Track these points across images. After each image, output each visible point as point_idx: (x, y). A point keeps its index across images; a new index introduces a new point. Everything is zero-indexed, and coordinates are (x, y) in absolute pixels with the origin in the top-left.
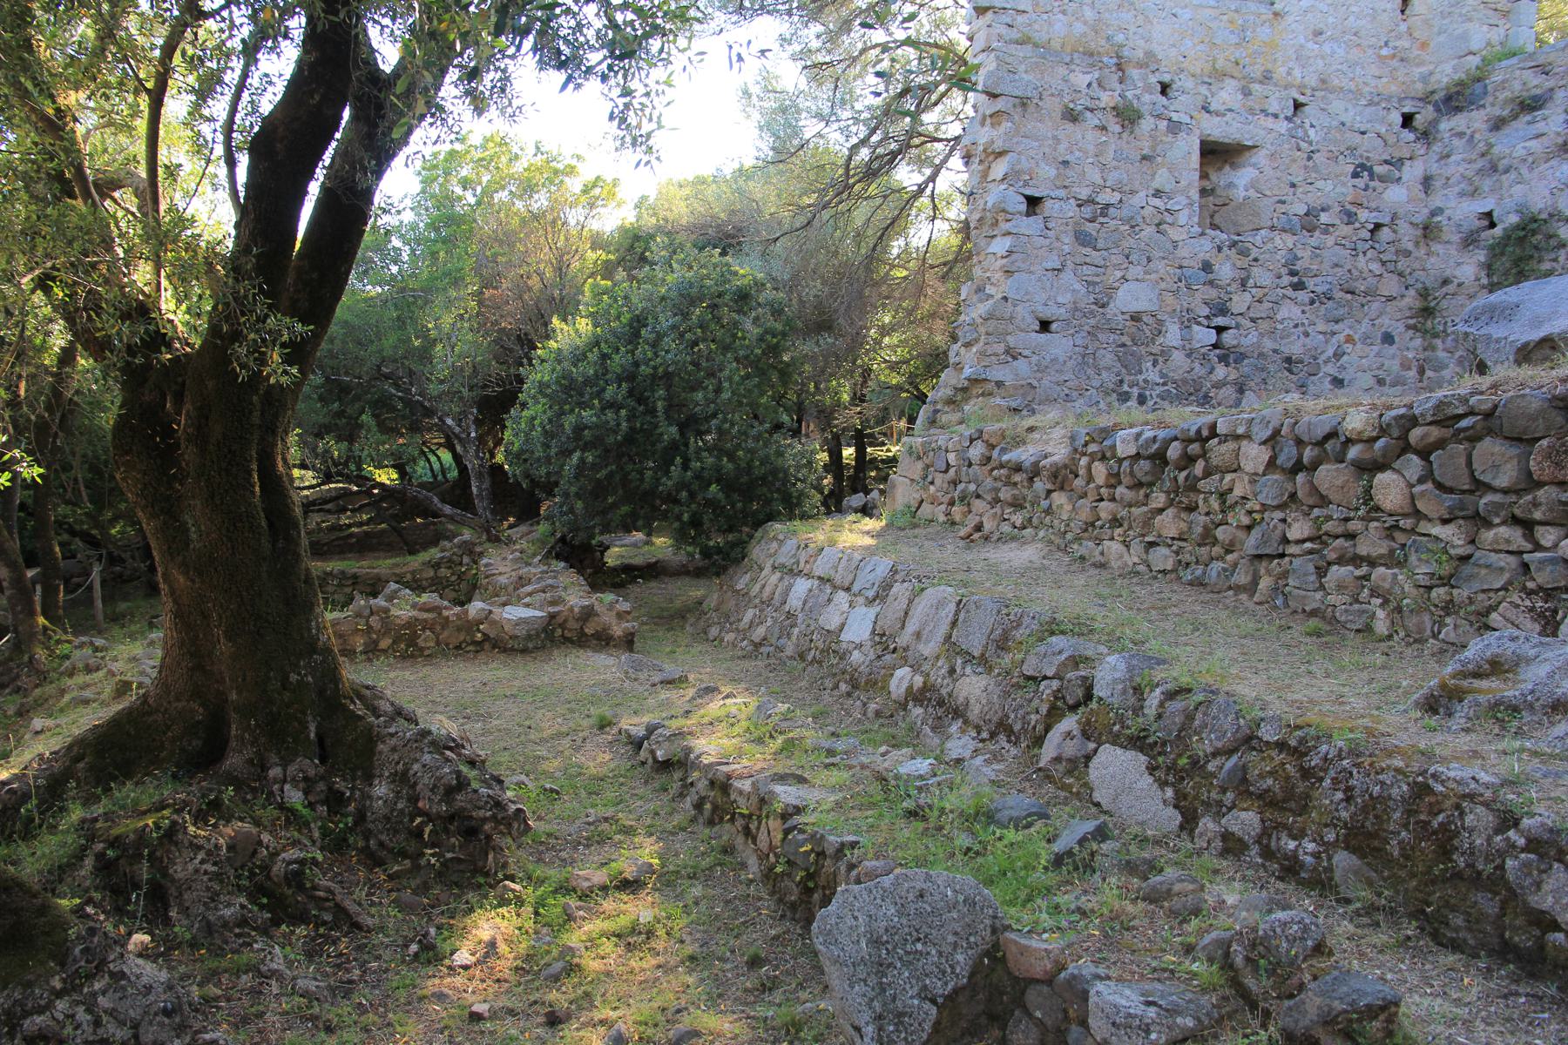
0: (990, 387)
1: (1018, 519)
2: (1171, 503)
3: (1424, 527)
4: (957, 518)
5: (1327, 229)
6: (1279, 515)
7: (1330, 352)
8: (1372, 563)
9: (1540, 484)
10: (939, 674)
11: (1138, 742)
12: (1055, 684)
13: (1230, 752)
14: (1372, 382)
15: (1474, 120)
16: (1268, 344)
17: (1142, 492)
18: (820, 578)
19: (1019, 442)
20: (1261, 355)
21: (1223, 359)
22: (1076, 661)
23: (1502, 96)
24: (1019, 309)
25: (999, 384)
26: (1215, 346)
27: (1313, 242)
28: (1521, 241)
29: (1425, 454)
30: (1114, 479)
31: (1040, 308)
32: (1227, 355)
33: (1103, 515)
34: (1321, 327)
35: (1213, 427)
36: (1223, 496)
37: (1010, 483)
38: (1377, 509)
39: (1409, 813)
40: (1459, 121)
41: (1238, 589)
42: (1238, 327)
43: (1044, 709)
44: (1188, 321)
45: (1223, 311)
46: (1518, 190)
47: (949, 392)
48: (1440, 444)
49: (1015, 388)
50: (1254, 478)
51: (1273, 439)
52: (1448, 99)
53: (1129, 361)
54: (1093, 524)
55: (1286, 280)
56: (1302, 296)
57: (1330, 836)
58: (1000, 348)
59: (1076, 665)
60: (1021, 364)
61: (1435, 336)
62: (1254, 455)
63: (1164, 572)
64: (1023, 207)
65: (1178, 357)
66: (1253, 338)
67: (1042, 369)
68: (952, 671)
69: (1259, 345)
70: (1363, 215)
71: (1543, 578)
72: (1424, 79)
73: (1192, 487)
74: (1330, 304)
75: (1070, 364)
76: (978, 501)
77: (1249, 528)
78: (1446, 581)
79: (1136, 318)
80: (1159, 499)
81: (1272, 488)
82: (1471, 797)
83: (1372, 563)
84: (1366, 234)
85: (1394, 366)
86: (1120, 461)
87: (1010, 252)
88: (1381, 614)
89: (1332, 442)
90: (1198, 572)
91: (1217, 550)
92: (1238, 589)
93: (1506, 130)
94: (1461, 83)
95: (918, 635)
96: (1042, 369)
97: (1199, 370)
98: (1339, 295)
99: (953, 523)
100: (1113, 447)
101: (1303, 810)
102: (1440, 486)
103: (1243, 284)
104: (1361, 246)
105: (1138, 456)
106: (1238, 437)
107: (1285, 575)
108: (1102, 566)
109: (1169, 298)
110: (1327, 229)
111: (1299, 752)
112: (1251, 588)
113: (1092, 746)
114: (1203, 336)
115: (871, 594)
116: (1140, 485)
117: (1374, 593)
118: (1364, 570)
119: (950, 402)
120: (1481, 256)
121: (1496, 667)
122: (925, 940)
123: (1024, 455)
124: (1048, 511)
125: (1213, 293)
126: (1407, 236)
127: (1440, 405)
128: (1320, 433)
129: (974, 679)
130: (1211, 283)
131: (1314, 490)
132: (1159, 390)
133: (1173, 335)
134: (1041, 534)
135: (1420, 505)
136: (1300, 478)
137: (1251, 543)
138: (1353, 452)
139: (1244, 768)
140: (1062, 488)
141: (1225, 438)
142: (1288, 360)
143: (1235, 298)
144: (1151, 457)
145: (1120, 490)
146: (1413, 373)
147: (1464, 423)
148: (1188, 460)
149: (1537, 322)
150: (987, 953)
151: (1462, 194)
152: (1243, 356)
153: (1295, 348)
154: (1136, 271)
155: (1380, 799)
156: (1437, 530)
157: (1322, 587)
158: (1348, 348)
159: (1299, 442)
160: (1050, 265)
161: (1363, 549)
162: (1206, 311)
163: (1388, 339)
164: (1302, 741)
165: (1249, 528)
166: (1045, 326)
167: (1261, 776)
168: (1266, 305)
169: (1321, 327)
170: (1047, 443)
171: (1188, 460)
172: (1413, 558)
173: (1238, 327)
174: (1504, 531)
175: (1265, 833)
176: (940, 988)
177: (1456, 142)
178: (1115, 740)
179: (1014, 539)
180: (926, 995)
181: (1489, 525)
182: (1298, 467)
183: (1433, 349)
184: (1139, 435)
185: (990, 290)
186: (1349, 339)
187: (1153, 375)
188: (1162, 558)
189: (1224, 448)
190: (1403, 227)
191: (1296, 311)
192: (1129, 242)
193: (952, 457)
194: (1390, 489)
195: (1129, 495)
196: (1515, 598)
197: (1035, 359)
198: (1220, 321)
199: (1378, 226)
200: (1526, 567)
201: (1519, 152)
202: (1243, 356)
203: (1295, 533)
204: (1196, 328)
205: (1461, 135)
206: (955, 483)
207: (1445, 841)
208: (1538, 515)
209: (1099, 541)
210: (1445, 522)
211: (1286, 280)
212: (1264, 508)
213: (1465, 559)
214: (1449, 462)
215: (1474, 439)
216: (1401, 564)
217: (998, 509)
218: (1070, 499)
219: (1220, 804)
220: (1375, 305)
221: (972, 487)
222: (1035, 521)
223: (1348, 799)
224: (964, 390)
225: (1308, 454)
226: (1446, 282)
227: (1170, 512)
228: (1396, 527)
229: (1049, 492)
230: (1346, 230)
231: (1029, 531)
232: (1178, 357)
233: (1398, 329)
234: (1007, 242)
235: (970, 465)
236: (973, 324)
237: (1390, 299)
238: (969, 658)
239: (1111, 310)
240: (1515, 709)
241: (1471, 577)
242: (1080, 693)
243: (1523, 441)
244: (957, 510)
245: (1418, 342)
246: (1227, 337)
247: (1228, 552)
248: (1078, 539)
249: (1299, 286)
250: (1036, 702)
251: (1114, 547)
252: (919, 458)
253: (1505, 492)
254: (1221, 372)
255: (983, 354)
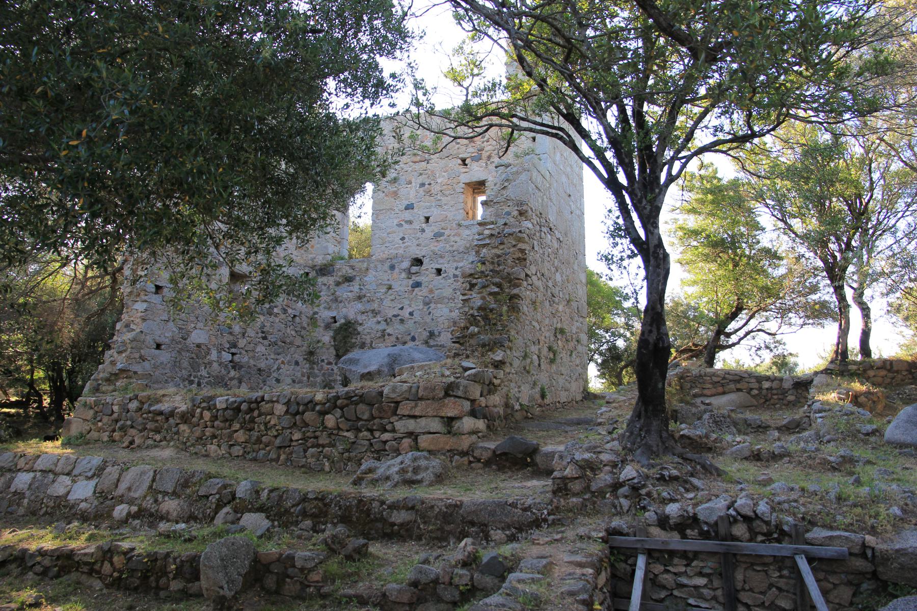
0: (131, 374)
1: (158, 437)
2: (242, 428)
3: (341, 433)
4: (117, 438)
5: (276, 315)
6: (289, 431)
7: (275, 367)
8: (323, 446)
9: (375, 418)
10: (148, 503)
11: (260, 509)
12: (217, 496)
13: (298, 505)
14: (291, 381)
15: (330, 280)
16: (252, 362)
17: (227, 424)
18: (41, 471)
19: (158, 401)
20: (249, 367)
21: (234, 367)
22: (225, 487)
23: (340, 274)
24: (148, 337)
25: (135, 373)
26: (231, 362)
27: (271, 320)
28: (346, 329)
29: (342, 408)
30: (215, 418)
31: (157, 338)
32: (236, 366)
33: (207, 434)
34: (272, 356)
35: (263, 397)
36: (266, 424)
37: (154, 420)
38: (326, 427)
39: (358, 508)
40: (324, 279)
41: (272, 460)
42: (240, 354)
43: (214, 506)
44: (220, 350)
45: (234, 345)
46: (344, 310)
47: (106, 375)
48: (347, 405)
49: (143, 375)
50: (279, 417)
51: (288, 403)
52: (321, 270)
53: (194, 366)
54: (201, 438)
55: (260, 335)
56: (266, 342)
57: (335, 521)
58: (137, 355)
59: (225, 488)
60: (146, 364)
61: (314, 363)
62: (280, 409)
63: (238, 456)
64: (154, 290)
65: (215, 365)
66: (246, 359)
67: (155, 367)
68: (156, 501)
69: (248, 362)
70: (290, 311)
71: (376, 447)
72: (313, 259)
73: (252, 420)
74: (276, 347)
75: (169, 365)
76: (132, 430)
77: (276, 437)
78: (348, 451)
79: (199, 346)
80: (236, 426)
81: (287, 421)
82: (373, 500)
83: (323, 446)
84: (290, 319)
85: (299, 375)
86: (218, 410)
87: (146, 310)
88: (327, 464)
89: (310, 404)
90: (254, 454)
91: (262, 446)
92: (272, 460)
93: (341, 287)
94: (325, 265)
95: (129, 489)
96: (155, 367)
97: (224, 372)
98: (280, 343)
99: (114, 441)
100: (215, 405)
101: (326, 516)
102: (346, 419)
103: (244, 335)
104: (289, 324)
105: (227, 408)
106: (273, 402)
107: (291, 453)
108: (207, 456)
109: (213, 338)
110: (276, 315)
111: (322, 499)
112: (277, 460)
113: (239, 515)
114: (227, 357)
115: (90, 474)
116: (227, 420)
117: (324, 457)
118: (321, 449)
119: (108, 380)
120: (331, 333)
121: (370, 471)
122: (236, 558)
123: (165, 406)
124: (177, 433)
125: (231, 338)
126: (305, 321)
127: (347, 393)
128: (306, 401)
129: (171, 502)
130: (231, 333)
131: (304, 421)
132: (206, 380)
133: (214, 355)
134: (172, 444)
135: (340, 426)
136: (298, 417)
137: (278, 442)
138: (318, 408)
139: (304, 508)
140: (185, 422)
141: (268, 402)
142: (259, 370)
143: (240, 341)
144: (233, 409)
145: (216, 423)
146: (305, 378)
147: (354, 399)
148: (251, 410)
149: (365, 367)
150: (253, 561)
151: (325, 308)
152: (242, 367)
153: (262, 365)
154: (200, 325)
155: (350, 506)
156: (345, 434)
157: (305, 457)
158: (282, 366)
159: (298, 404)
160: (163, 318)
161: (321, 442)
162: (228, 346)
163: (297, 363)
164: (323, 496)
165: (276, 437)
166: (158, 346)
167: (311, 509)
168: (252, 345)
169: (272, 356)
170: (174, 402)
171: (251, 410)
172: (338, 444)
173: (240, 354)
174: (365, 433)
175: (314, 526)
176: (243, 572)
177: (323, 287)
178: (250, 511)
179: (156, 446)
180: (239, 574)
181: (361, 431)
182: (298, 413)
183: (313, 368)
184: (227, 400)
185: (132, 326)
186: (283, 363)
187: (204, 373)
188: (238, 450)
189: (267, 406)
190: (304, 318)
191: (263, 348)
192: (198, 312)
193: (116, 408)
194: (330, 421)
195: (222, 425)
196: (369, 454)
197: (153, 362)
198: (233, 350)
199: (295, 316)
200: (371, 444)
201: (345, 296)
202: (242, 367)
203: (295, 437)
204: (223, 353)
205: (325, 285)
206: (117, 421)
207: (368, 512)
208: (375, 428)
209: (205, 445)
210: (348, 431)
211: (260, 335)
212: (283, 428)
213: (354, 443)
214: (349, 411)
215: (357, 404)
216: (333, 446)
217: (145, 433)
218: (189, 427)
219: (297, 521)
220: (293, 349)
221: (129, 423)
222: (168, 438)
223: (340, 509)
224: (116, 374)
225: (301, 408)
226: (319, 342)
227: (242, 431)
228: (332, 434)
229: (178, 424)
230: (283, 316)
231: (164, 443)
232: (215, 365)
233: (300, 359)
234: (145, 305)
235: (128, 411)
236: (124, 342)
237: (298, 347)
238: (165, 493)
239: (188, 341)
240: (377, 481)
241: (356, 448)
242: (230, 497)
243: (371, 405)
244: (116, 435)
245: (307, 365)
246: (236, 358)
247: (267, 446)
248: (193, 445)
249: (265, 338)
250: (209, 505)
251: (213, 447)
252: (91, 408)
253: (366, 420)
254: (233, 373)
255: (128, 357)
